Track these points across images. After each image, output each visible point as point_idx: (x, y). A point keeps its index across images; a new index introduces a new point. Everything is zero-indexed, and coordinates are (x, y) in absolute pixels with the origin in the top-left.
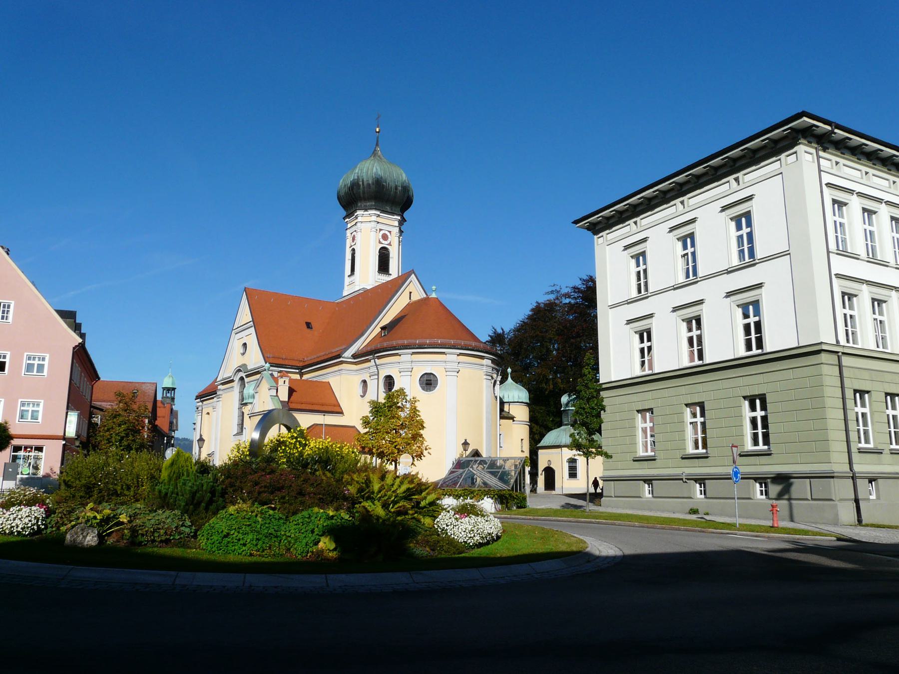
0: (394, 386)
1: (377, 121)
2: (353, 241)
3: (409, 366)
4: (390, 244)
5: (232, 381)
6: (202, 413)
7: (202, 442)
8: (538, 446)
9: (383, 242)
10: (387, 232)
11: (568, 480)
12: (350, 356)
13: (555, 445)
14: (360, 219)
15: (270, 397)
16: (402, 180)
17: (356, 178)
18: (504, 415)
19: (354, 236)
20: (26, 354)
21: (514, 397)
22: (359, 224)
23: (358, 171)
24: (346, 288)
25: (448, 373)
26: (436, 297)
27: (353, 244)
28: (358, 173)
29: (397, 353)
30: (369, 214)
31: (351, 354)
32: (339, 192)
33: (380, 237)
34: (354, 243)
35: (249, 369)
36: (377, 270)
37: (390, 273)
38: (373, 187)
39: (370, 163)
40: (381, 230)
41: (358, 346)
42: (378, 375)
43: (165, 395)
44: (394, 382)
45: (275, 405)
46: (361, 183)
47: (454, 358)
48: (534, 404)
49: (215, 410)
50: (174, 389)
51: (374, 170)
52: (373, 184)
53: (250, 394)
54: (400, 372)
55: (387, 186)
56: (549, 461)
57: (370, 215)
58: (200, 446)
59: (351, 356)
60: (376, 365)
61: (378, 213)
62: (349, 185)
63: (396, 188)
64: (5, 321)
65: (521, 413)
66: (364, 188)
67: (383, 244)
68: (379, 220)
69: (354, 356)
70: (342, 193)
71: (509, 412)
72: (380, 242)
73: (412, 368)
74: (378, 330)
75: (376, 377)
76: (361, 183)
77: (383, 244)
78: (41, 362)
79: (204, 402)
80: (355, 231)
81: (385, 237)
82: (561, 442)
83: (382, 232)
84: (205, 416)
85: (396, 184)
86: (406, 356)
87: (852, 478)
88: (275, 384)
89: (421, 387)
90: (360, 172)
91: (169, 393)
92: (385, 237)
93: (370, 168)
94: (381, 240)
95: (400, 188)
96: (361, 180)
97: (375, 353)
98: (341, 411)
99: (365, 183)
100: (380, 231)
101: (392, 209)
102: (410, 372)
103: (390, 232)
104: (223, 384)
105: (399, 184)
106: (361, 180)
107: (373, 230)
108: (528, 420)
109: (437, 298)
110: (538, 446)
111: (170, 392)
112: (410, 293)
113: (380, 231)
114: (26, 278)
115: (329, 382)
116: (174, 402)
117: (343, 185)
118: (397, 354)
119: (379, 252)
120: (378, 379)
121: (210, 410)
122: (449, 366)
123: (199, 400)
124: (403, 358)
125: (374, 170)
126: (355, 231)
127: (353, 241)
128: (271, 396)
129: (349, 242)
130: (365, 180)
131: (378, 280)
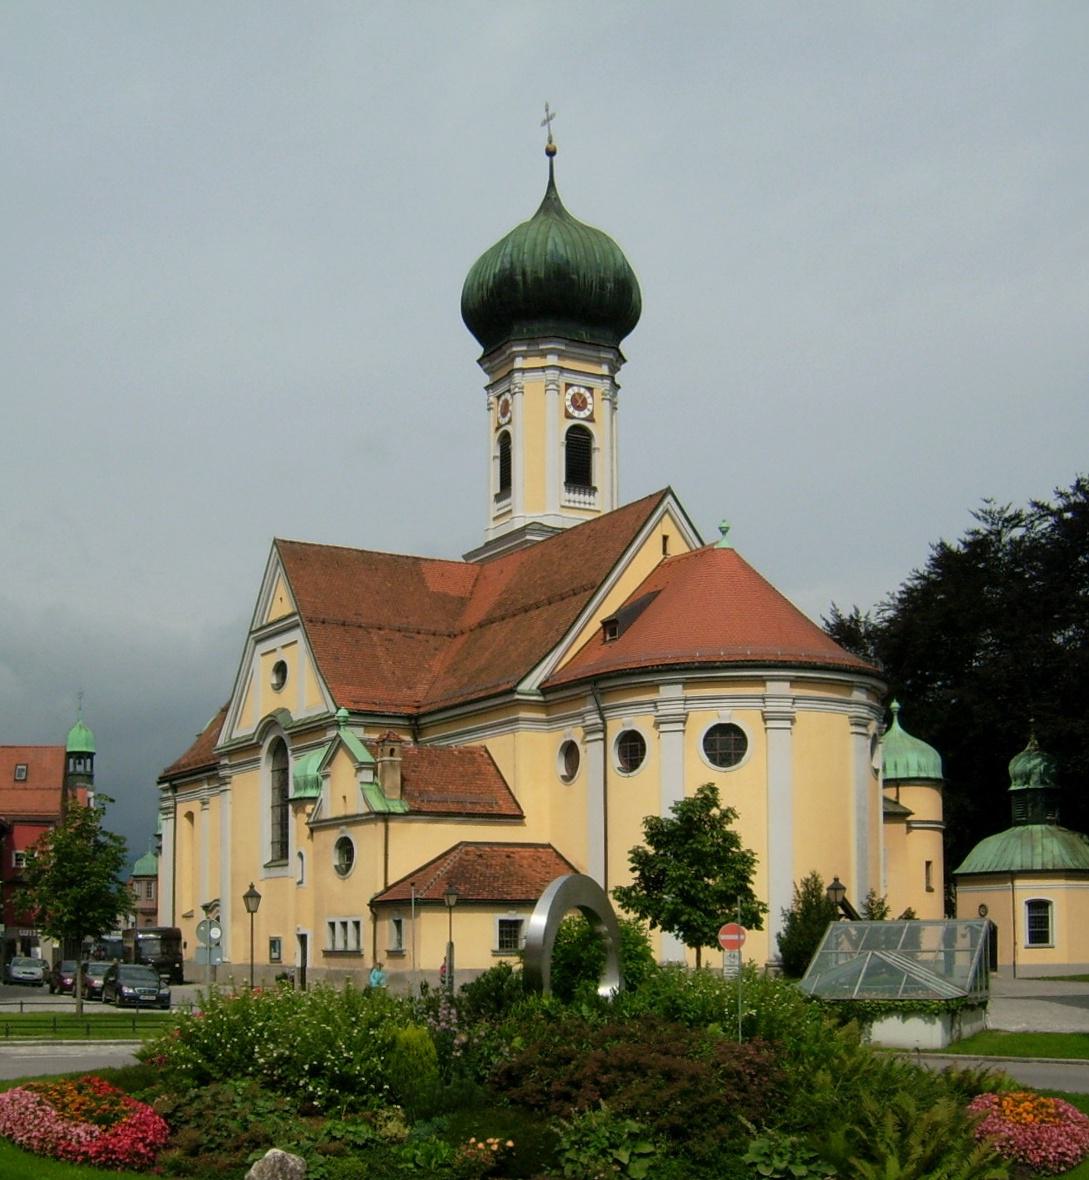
1: (546, 127)
2: (504, 414)
4: (590, 419)
6: (175, 813)
7: (255, 900)
8: (956, 872)
9: (576, 414)
10: (582, 391)
11: (1027, 948)
12: (534, 688)
13: (997, 870)
14: (519, 363)
15: (360, 786)
17: (508, 266)
18: (895, 814)
19: (506, 403)
21: (907, 766)
22: (517, 376)
23: (512, 251)
25: (770, 724)
27: (503, 421)
28: (511, 255)
31: (537, 684)
33: (568, 403)
34: (507, 419)
35: (295, 719)
36: (564, 479)
37: (594, 484)
39: (538, 229)
40: (568, 386)
41: (551, 665)
42: (604, 730)
43: (71, 769)
47: (783, 688)
48: (950, 785)
49: (205, 807)
50: (90, 755)
51: (550, 246)
53: (310, 778)
55: (581, 280)
56: (982, 906)
57: (543, 354)
58: (252, 909)
59: (538, 688)
62: (491, 284)
63: (602, 287)
65: (925, 804)
66: (525, 282)
67: (573, 418)
69: (545, 689)
71: (897, 803)
72: (569, 416)
73: (687, 715)
74: (595, 625)
75: (600, 735)
77: (573, 418)
80: (509, 391)
82: (1012, 864)
83: (571, 391)
84: (183, 822)
85: (602, 275)
88: (370, 757)
89: (708, 755)
91: (80, 763)
92: (579, 403)
94: (571, 410)
95: (610, 285)
98: (517, 813)
99: (529, 278)
100: (566, 390)
101: (592, 336)
102: (681, 724)
103: (590, 389)
104: (229, 754)
105: (610, 275)
106: (518, 271)
107: (551, 387)
108: (941, 819)
110: (956, 872)
111: (82, 761)
112: (665, 538)
113: (566, 390)
114: (1045, 962)
115: (485, 747)
116: (92, 784)
117: (476, 284)
119: (568, 437)
120: (604, 740)
121: (194, 806)
122: (772, 706)
123: (166, 785)
125: (550, 246)
126: (509, 391)
127: (504, 414)
128: (362, 783)
130: (528, 269)
131: (567, 504)
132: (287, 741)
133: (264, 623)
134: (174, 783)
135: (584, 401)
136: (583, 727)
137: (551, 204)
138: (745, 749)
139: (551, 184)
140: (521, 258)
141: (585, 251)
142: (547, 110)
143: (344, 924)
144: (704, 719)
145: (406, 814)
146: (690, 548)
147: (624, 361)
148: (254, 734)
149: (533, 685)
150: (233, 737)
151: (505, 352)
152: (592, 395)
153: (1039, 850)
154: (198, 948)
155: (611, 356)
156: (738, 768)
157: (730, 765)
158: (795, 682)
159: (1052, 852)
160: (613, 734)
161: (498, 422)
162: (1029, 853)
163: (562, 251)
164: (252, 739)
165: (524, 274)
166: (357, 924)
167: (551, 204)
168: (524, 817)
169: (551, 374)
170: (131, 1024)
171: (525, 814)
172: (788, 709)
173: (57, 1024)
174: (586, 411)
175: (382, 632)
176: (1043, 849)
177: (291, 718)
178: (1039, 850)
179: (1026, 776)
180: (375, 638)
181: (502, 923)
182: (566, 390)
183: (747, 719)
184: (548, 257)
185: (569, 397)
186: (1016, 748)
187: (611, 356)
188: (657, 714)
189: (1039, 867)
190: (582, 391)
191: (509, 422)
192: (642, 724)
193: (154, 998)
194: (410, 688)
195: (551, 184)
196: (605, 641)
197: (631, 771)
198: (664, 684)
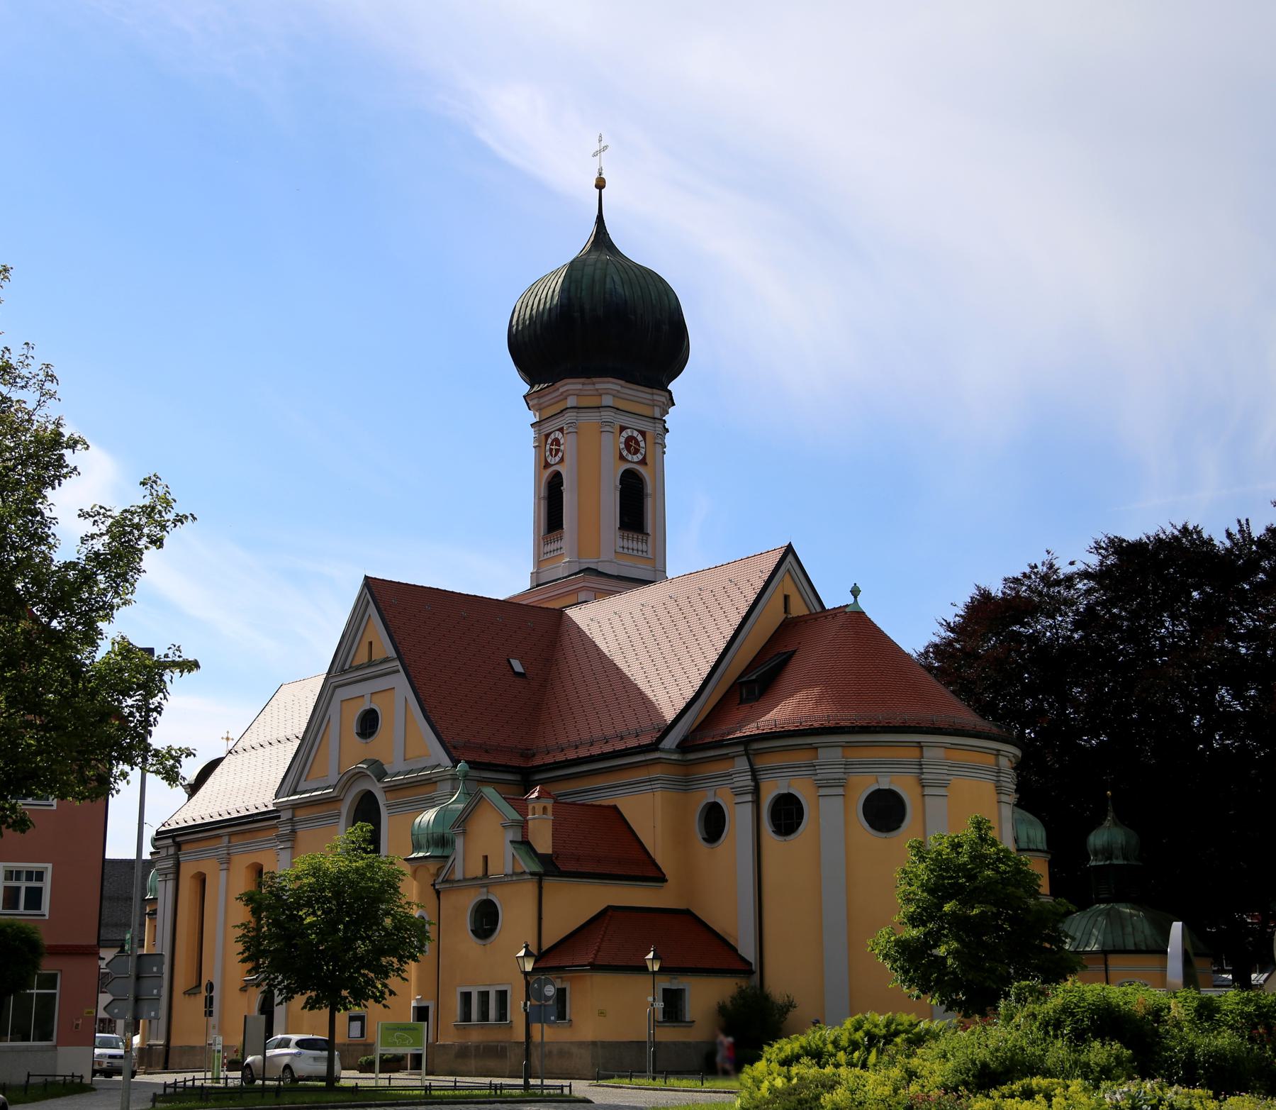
9: (629, 457)
10: (635, 434)
33: (622, 446)
34: (557, 459)
36: (618, 525)
40: (622, 429)
46: (577, 315)
76: (577, 315)
83: (625, 434)
103: (643, 433)
132: (381, 799)
134: (178, 839)
137: (601, 238)
138: (802, 818)
139: (600, 219)
140: (579, 295)
142: (600, 141)
144: (865, 784)
146: (809, 610)
147: (673, 404)
151: (558, 389)
153: (1129, 929)
155: (663, 399)
159: (1143, 932)
160: (768, 796)
163: (620, 290)
166: (502, 995)
167: (601, 238)
169: (607, 415)
174: (639, 455)
176: (1133, 928)
178: (1129, 929)
179: (1107, 852)
182: (621, 433)
183: (904, 785)
185: (623, 440)
186: (1096, 823)
187: (663, 399)
188: (817, 778)
189: (1133, 948)
190: (635, 434)
192: (801, 789)
195: (600, 219)
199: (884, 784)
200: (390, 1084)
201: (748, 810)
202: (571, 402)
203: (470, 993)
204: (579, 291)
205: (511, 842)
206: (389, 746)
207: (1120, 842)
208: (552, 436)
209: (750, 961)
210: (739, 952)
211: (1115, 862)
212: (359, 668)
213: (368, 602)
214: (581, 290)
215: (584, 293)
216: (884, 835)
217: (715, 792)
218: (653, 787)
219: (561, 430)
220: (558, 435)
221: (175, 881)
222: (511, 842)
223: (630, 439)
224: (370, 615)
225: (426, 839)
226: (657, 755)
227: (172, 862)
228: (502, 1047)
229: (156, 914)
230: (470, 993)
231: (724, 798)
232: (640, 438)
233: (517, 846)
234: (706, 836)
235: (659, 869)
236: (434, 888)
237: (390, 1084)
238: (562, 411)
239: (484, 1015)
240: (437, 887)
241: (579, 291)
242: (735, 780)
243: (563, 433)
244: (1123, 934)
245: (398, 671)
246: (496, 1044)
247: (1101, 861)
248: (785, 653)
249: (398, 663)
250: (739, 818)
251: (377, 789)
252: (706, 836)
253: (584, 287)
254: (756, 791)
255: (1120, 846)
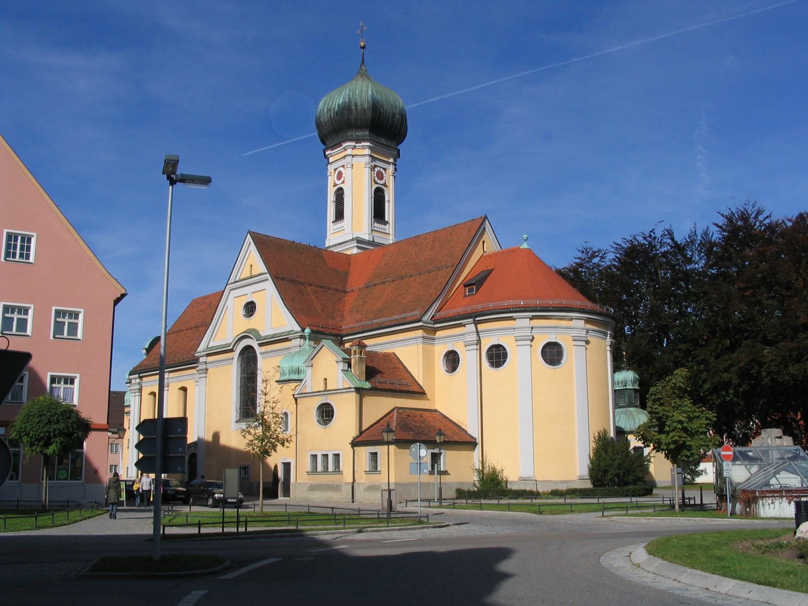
0: (459, 363)
3: (528, 332)
5: (232, 351)
16: (400, 107)
17: (347, 100)
20: (54, 308)
24: (251, 240)
25: (468, 348)
26: (528, 247)
28: (349, 95)
29: (512, 317)
30: (363, 146)
32: (320, 118)
34: (341, 181)
35: (262, 335)
38: (369, 113)
44: (459, 358)
45: (154, 385)
46: (353, 107)
51: (370, 93)
52: (369, 108)
54: (466, 346)
60: (477, 332)
61: (353, 144)
64: (24, 260)
67: (378, 184)
68: (355, 152)
70: (325, 118)
76: (353, 107)
77: (378, 184)
78: (22, 316)
79: (144, 379)
81: (380, 176)
86: (523, 322)
87: (442, 499)
90: (351, 94)
93: (363, 89)
96: (353, 103)
97: (476, 317)
98: (422, 391)
99: (359, 108)
103: (385, 169)
104: (208, 355)
105: (397, 111)
106: (353, 103)
109: (530, 249)
118: (511, 318)
123: (137, 376)
124: (519, 323)
129: (332, 179)
130: (359, 104)
132: (258, 350)
133: (237, 279)
134: (141, 375)
135: (382, 174)
136: (464, 342)
141: (386, 97)
143: (326, 456)
145: (370, 389)
148: (231, 343)
149: (428, 319)
150: (209, 346)
152: (386, 172)
154: (411, 463)
156: (503, 369)
157: (500, 366)
158: (587, 321)
161: (335, 183)
162: (633, 422)
164: (230, 346)
165: (356, 105)
166: (337, 456)
168: (426, 394)
170: (662, 499)
171: (426, 392)
172: (585, 335)
173: (225, 520)
174: (383, 180)
175: (312, 287)
176: (639, 420)
177: (260, 335)
180: (309, 290)
181: (432, 453)
184: (369, 98)
190: (381, 170)
191: (343, 182)
192: (507, 342)
193: (235, 500)
194: (333, 319)
196: (465, 296)
197: (452, 372)
198: (467, 324)
199: (553, 339)
200: (598, 501)
201: (474, 354)
202: (349, 151)
203: (316, 455)
204: (354, 95)
205: (342, 370)
206: (258, 322)
207: (630, 377)
208: (338, 170)
209: (475, 437)
210: (468, 432)
211: (628, 387)
212: (244, 279)
213: (250, 243)
214: (356, 95)
215: (357, 96)
216: (553, 367)
217: (453, 345)
218: (418, 341)
219: (343, 166)
220: (341, 169)
221: (140, 397)
222: (342, 370)
223: (378, 172)
224: (251, 251)
225: (288, 370)
226: (420, 324)
227: (496, 250)
228: (336, 485)
229: (129, 413)
230: (316, 455)
231: (460, 349)
232: (376, 179)
233: (345, 372)
234: (447, 369)
235: (422, 388)
236: (294, 397)
237: (598, 501)
238: (344, 157)
239: (326, 468)
240: (295, 396)
241: (354, 95)
242: (466, 337)
243: (344, 168)
244: (634, 423)
245: (268, 280)
246: (333, 483)
247: (621, 387)
248: (488, 270)
249: (268, 275)
250: (469, 358)
251: (254, 344)
252: (447, 369)
253: (357, 94)
254: (479, 342)
255: (630, 379)
